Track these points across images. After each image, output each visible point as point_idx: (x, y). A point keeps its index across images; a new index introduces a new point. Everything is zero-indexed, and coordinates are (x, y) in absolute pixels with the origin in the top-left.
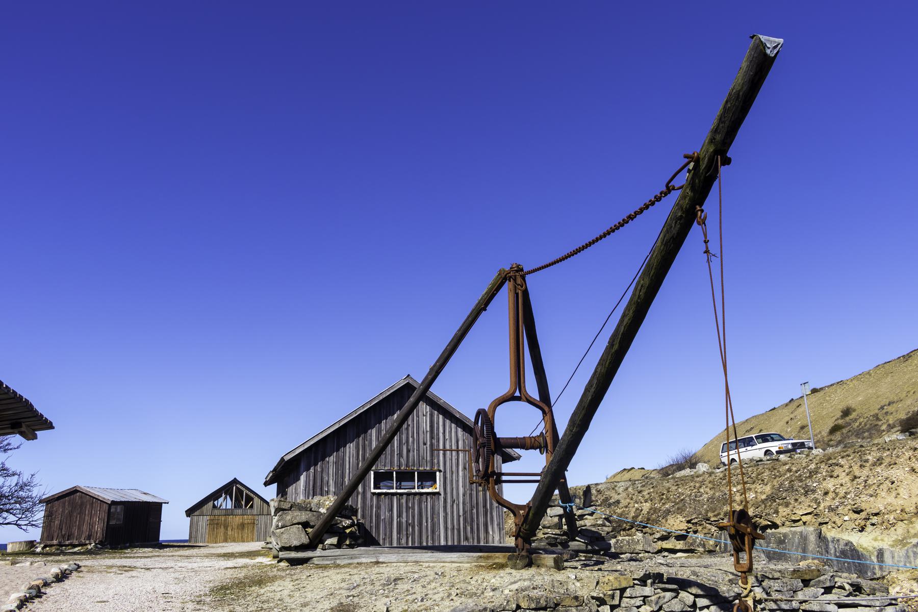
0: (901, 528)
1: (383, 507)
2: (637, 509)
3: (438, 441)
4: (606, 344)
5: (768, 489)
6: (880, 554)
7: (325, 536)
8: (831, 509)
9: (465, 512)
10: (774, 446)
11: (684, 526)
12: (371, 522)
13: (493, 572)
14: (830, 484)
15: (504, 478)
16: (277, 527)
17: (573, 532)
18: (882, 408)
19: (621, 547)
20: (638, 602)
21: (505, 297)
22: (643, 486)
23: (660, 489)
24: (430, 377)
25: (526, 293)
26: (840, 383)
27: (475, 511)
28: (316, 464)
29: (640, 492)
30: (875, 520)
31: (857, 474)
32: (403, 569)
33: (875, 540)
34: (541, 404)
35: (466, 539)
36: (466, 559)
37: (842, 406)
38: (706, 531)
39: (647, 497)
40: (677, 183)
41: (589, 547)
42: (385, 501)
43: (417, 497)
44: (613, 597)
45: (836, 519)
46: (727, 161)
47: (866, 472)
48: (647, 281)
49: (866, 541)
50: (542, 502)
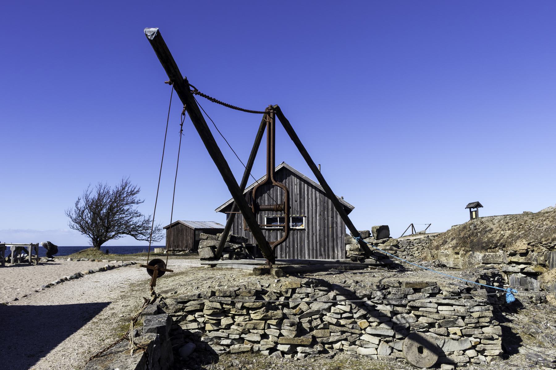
1: (272, 237)
2: (502, 235)
7: (223, 253)
9: (320, 240)
11: (525, 247)
19: (488, 259)
22: (511, 219)
27: (326, 239)
29: (507, 223)
38: (539, 251)
39: (510, 226)
41: (378, 263)
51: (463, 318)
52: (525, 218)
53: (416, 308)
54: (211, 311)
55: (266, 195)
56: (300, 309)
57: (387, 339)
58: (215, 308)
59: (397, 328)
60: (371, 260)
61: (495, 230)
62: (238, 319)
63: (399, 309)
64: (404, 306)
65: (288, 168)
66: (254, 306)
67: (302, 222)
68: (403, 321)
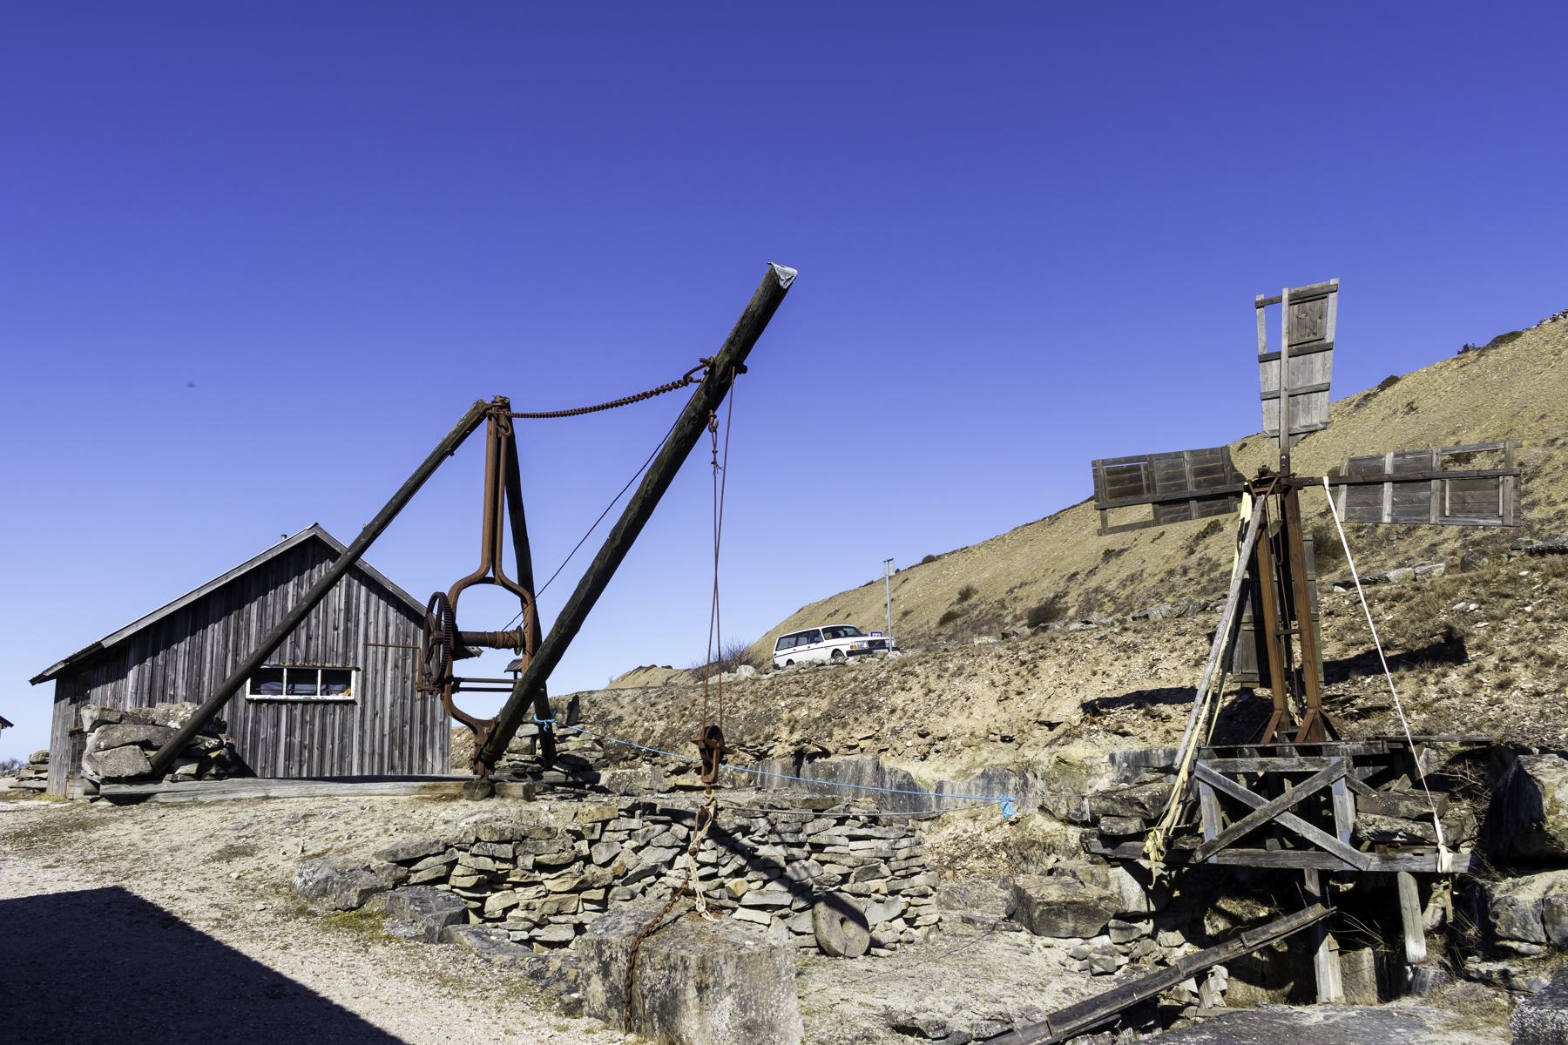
0: (967, 755)
3: (357, 625)
4: (606, 536)
5: (824, 704)
6: (940, 787)
8: (895, 732)
9: (392, 730)
10: (845, 644)
12: (244, 742)
13: (443, 805)
14: (899, 700)
15: (462, 685)
16: (98, 748)
17: (550, 757)
18: (1011, 591)
20: (623, 836)
21: (481, 438)
23: (683, 701)
24: (363, 540)
25: (511, 440)
26: (965, 550)
27: (407, 728)
28: (155, 654)
29: (653, 705)
30: (940, 745)
31: (933, 687)
32: (310, 805)
33: (937, 770)
34: (521, 590)
35: (392, 768)
36: (403, 790)
37: (961, 585)
38: (738, 761)
39: (663, 712)
40: (695, 376)
42: (267, 714)
43: (319, 708)
44: (592, 830)
45: (898, 744)
46: (743, 370)
47: (943, 684)
48: (656, 477)
49: (925, 772)
50: (512, 718)
51: (887, 860)
52: (693, 696)
53: (818, 848)
54: (474, 880)
55: (254, 607)
56: (622, 864)
57: (783, 912)
58: (481, 872)
59: (798, 889)
60: (555, 774)
61: (628, 720)
62: (524, 895)
63: (795, 851)
64: (800, 845)
65: (325, 540)
66: (560, 861)
67: (349, 685)
68: (804, 874)
